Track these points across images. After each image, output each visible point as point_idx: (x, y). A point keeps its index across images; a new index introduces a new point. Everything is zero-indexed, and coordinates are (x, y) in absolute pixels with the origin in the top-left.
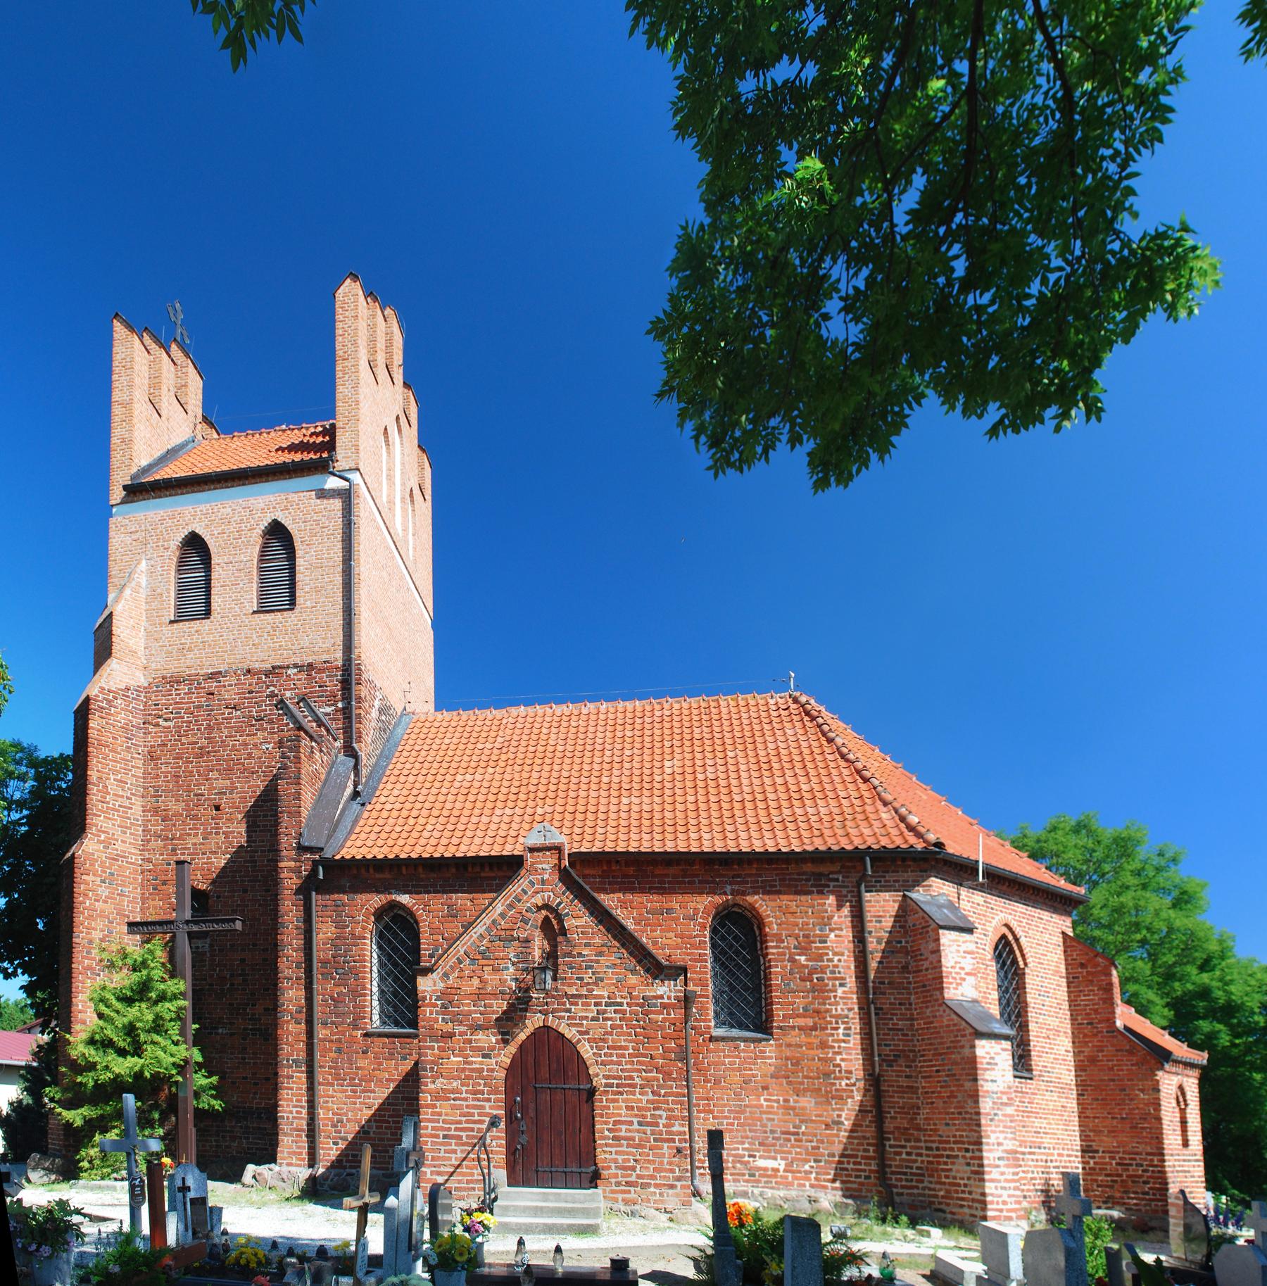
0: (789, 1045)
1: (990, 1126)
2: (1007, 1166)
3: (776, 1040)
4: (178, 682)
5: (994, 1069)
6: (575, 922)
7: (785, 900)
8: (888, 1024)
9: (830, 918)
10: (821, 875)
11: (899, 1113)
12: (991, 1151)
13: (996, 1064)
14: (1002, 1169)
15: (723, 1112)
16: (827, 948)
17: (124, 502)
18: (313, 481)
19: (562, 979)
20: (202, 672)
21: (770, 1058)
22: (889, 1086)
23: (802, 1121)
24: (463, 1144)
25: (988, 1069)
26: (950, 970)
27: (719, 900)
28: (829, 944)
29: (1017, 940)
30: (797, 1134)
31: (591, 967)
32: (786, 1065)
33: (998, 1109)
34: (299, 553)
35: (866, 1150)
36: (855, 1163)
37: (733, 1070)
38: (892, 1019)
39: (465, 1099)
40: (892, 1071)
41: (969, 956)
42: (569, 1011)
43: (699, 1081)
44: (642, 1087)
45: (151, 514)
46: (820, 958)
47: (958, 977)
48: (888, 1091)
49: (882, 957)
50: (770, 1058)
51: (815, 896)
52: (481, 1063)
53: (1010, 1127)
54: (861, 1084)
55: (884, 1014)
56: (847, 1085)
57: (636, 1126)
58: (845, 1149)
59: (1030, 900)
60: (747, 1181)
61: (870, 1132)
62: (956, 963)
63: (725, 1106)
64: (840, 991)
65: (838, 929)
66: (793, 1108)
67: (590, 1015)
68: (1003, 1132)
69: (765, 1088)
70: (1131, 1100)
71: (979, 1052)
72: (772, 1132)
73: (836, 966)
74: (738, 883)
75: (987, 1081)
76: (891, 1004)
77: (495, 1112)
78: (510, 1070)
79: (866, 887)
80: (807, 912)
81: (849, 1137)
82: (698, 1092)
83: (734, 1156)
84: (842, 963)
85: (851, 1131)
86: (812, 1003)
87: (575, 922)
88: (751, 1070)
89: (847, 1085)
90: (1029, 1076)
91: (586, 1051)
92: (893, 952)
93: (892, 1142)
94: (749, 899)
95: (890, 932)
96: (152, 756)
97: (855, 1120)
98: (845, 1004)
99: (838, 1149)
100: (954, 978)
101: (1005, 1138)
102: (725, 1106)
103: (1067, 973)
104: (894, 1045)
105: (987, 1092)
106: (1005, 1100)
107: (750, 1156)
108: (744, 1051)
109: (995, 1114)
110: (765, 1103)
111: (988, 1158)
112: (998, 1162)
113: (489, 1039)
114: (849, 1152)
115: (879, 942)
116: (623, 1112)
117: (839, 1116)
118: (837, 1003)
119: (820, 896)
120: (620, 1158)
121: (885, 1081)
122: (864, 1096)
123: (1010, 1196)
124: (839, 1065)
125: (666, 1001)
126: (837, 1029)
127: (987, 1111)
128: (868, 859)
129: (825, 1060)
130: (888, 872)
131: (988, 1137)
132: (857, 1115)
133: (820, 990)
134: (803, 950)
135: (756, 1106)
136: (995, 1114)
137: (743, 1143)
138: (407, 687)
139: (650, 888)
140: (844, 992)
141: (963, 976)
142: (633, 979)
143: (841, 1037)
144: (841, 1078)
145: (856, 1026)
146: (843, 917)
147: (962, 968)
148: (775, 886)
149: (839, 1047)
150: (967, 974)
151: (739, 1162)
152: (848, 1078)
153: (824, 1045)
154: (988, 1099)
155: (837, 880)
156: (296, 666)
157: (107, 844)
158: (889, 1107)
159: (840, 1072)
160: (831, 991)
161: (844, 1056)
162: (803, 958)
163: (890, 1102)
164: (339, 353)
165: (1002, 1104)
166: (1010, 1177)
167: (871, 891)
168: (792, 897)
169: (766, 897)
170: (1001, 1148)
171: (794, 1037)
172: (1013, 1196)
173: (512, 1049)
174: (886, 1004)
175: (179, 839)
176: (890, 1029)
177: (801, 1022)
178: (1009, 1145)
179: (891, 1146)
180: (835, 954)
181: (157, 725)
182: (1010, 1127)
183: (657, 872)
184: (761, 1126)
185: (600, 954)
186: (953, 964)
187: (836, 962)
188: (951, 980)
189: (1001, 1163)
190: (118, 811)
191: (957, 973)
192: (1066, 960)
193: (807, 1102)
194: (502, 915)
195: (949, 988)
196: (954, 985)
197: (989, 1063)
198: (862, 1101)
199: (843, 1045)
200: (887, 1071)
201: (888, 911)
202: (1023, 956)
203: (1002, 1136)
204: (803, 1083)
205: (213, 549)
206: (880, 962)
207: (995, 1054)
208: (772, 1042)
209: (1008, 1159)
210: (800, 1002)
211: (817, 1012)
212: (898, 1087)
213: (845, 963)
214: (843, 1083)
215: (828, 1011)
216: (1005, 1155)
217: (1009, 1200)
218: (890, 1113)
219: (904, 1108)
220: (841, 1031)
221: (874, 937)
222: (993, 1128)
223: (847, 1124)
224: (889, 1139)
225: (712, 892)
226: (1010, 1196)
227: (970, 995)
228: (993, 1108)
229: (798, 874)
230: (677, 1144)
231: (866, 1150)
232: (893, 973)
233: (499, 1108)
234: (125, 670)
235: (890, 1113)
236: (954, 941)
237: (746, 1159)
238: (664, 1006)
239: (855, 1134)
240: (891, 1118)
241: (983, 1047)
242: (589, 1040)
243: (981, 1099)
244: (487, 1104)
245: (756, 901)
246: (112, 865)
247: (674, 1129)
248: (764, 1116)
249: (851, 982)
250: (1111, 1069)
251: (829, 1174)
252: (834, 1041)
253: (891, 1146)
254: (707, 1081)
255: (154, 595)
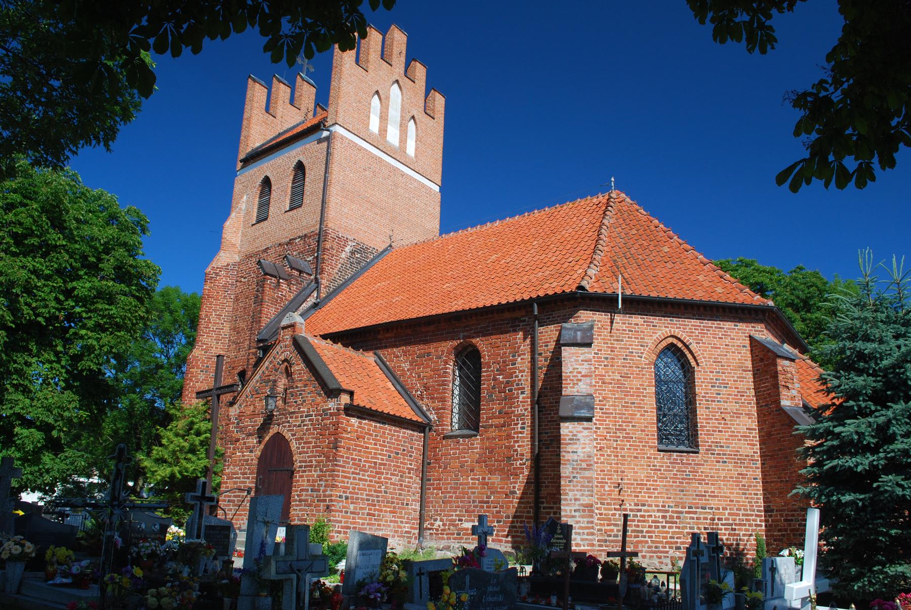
0: (488, 439)
1: (570, 486)
2: (582, 517)
3: (481, 435)
4: (251, 257)
5: (576, 444)
6: (297, 368)
7: (493, 339)
8: (547, 418)
9: (519, 347)
10: (516, 319)
11: (551, 482)
12: (568, 505)
13: (579, 439)
14: (578, 519)
15: (446, 488)
16: (515, 368)
17: (242, 168)
18: (315, 136)
19: (288, 403)
20: (261, 249)
21: (476, 448)
22: (546, 463)
23: (491, 493)
24: (235, 506)
25: (570, 444)
26: (569, 374)
27: (455, 343)
28: (517, 365)
29: (687, 347)
30: (488, 502)
31: (301, 394)
32: (485, 454)
33: (577, 473)
34: (307, 175)
35: (529, 512)
36: (521, 522)
37: (455, 458)
38: (550, 414)
39: (239, 478)
40: (548, 452)
41: (586, 363)
42: (288, 422)
43: (435, 467)
44: (316, 466)
45: (251, 171)
46: (511, 375)
47: (575, 379)
48: (545, 467)
49: (547, 370)
50: (476, 448)
51: (511, 334)
52: (248, 456)
53: (587, 487)
54: (528, 463)
55: (546, 411)
56: (520, 464)
57: (310, 492)
58: (516, 512)
59: (683, 314)
60: (455, 539)
61: (531, 498)
62: (574, 369)
63: (448, 484)
64: (521, 396)
65: (522, 354)
66: (487, 484)
67: (298, 424)
68: (581, 490)
69: (472, 470)
70: (791, 465)
71: (563, 431)
72: (474, 502)
73: (520, 380)
74: (467, 331)
75: (569, 452)
76: (550, 403)
77: (250, 485)
78: (260, 459)
79: (539, 323)
80: (506, 345)
81: (519, 503)
82: (432, 475)
83: (450, 520)
84: (524, 378)
85: (521, 498)
86: (504, 408)
87: (297, 368)
88: (465, 457)
89: (520, 464)
90: (697, 450)
91: (294, 445)
92: (553, 366)
93: (545, 505)
94: (474, 341)
95: (553, 352)
96: (237, 299)
97: (524, 490)
98: (523, 406)
99: (512, 511)
100: (573, 380)
101: (583, 495)
102: (448, 484)
103: (753, 367)
104: (551, 433)
105: (569, 460)
106: (584, 465)
107: (460, 520)
108: (462, 445)
109: (574, 477)
110: (471, 481)
111: (565, 511)
112: (573, 513)
113: (253, 441)
114: (518, 514)
115: (546, 361)
116: (305, 483)
117: (514, 487)
118: (518, 406)
119: (514, 333)
120: (300, 513)
121: (543, 459)
122: (530, 471)
123: (582, 540)
124: (516, 451)
125: (332, 411)
126: (517, 424)
127: (567, 474)
128: (536, 305)
129: (509, 448)
130: (554, 311)
131: (566, 494)
132: (525, 486)
133: (510, 399)
134: (501, 371)
135: (466, 484)
136: (574, 477)
137: (456, 511)
138: (391, 233)
139: (420, 341)
140: (523, 398)
141: (579, 378)
142: (319, 399)
143: (519, 430)
144: (517, 460)
145: (528, 422)
146: (525, 347)
147: (580, 373)
148: (489, 330)
149: (518, 437)
150: (582, 376)
151: (453, 525)
152: (521, 460)
153: (509, 437)
154: (568, 466)
155: (525, 321)
156: (299, 237)
157: (206, 351)
158: (545, 479)
159: (517, 455)
160: (516, 398)
161: (520, 444)
162: (501, 377)
163: (546, 475)
164: (334, 65)
165: (581, 469)
166: (585, 525)
167: (543, 326)
168: (498, 336)
169: (484, 338)
170: (577, 503)
171: (492, 433)
172: (587, 539)
173: (262, 446)
174: (547, 403)
175: (242, 343)
176: (549, 421)
177: (496, 421)
178: (586, 500)
179: (544, 508)
180: (520, 371)
181: (241, 282)
182: (587, 487)
183: (423, 330)
184: (468, 498)
185: (306, 386)
186: (571, 370)
187: (520, 377)
188: (568, 382)
189: (577, 514)
190: (215, 331)
191: (574, 376)
192: (752, 357)
193: (496, 479)
194: (267, 368)
195: (567, 388)
196: (571, 385)
197: (570, 439)
198: (529, 475)
199: (520, 435)
200: (545, 452)
201: (552, 338)
202: (694, 358)
203: (579, 493)
204: (494, 465)
205: (273, 183)
206: (545, 374)
207: (577, 432)
208: (478, 437)
209: (584, 511)
210: (496, 408)
211: (506, 413)
212: (551, 463)
213: (524, 378)
214: (518, 463)
215: (513, 412)
216: (581, 508)
217: (581, 543)
218: (545, 483)
219: (553, 479)
220: (519, 426)
221: (542, 357)
222: (572, 488)
223: (519, 493)
224: (543, 503)
225: (453, 339)
226: (582, 540)
227: (584, 391)
228: (573, 472)
229: (502, 320)
230: (327, 503)
231: (529, 512)
232: (553, 381)
233: (252, 482)
234: (228, 255)
235: (545, 483)
236: (573, 354)
237: (457, 522)
238: (331, 414)
239: (523, 500)
240: (546, 486)
241: (568, 427)
242: (296, 439)
243: (561, 466)
244: (248, 480)
245: (478, 342)
246: (208, 361)
247: (327, 493)
248: (470, 491)
249: (528, 390)
250: (779, 441)
251: (505, 531)
252: (515, 433)
253: (544, 508)
254: (440, 467)
255: (248, 213)
